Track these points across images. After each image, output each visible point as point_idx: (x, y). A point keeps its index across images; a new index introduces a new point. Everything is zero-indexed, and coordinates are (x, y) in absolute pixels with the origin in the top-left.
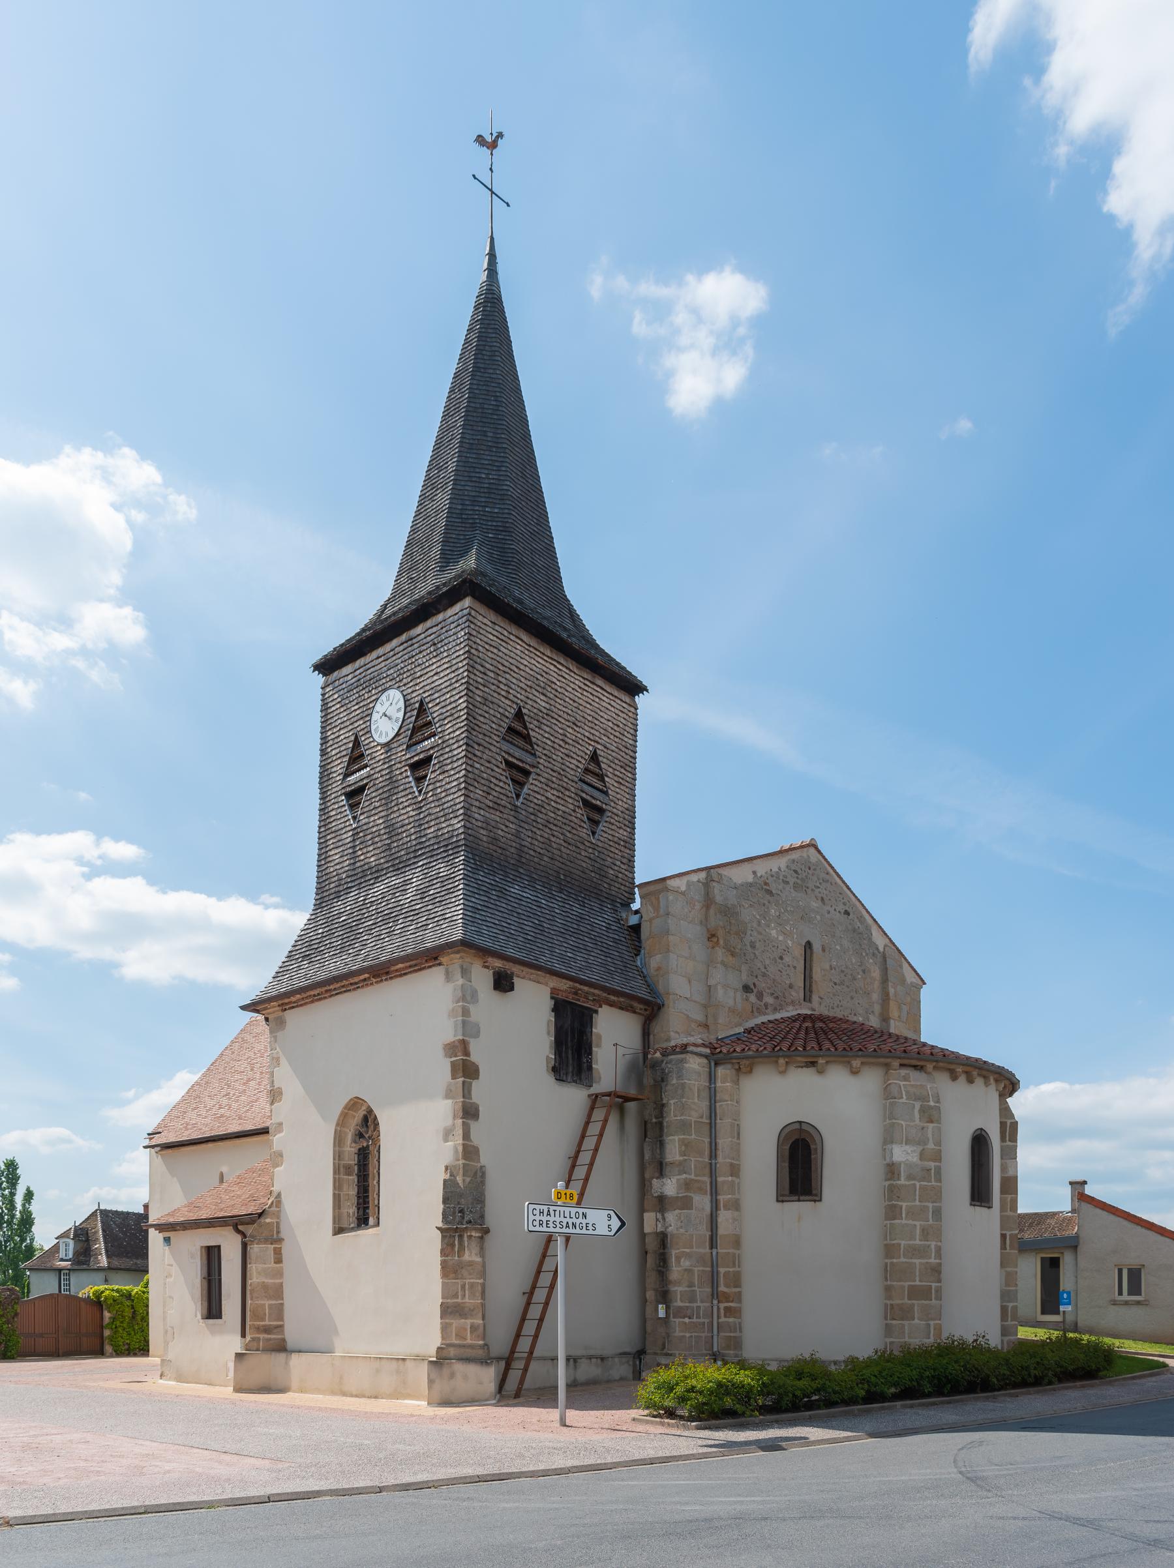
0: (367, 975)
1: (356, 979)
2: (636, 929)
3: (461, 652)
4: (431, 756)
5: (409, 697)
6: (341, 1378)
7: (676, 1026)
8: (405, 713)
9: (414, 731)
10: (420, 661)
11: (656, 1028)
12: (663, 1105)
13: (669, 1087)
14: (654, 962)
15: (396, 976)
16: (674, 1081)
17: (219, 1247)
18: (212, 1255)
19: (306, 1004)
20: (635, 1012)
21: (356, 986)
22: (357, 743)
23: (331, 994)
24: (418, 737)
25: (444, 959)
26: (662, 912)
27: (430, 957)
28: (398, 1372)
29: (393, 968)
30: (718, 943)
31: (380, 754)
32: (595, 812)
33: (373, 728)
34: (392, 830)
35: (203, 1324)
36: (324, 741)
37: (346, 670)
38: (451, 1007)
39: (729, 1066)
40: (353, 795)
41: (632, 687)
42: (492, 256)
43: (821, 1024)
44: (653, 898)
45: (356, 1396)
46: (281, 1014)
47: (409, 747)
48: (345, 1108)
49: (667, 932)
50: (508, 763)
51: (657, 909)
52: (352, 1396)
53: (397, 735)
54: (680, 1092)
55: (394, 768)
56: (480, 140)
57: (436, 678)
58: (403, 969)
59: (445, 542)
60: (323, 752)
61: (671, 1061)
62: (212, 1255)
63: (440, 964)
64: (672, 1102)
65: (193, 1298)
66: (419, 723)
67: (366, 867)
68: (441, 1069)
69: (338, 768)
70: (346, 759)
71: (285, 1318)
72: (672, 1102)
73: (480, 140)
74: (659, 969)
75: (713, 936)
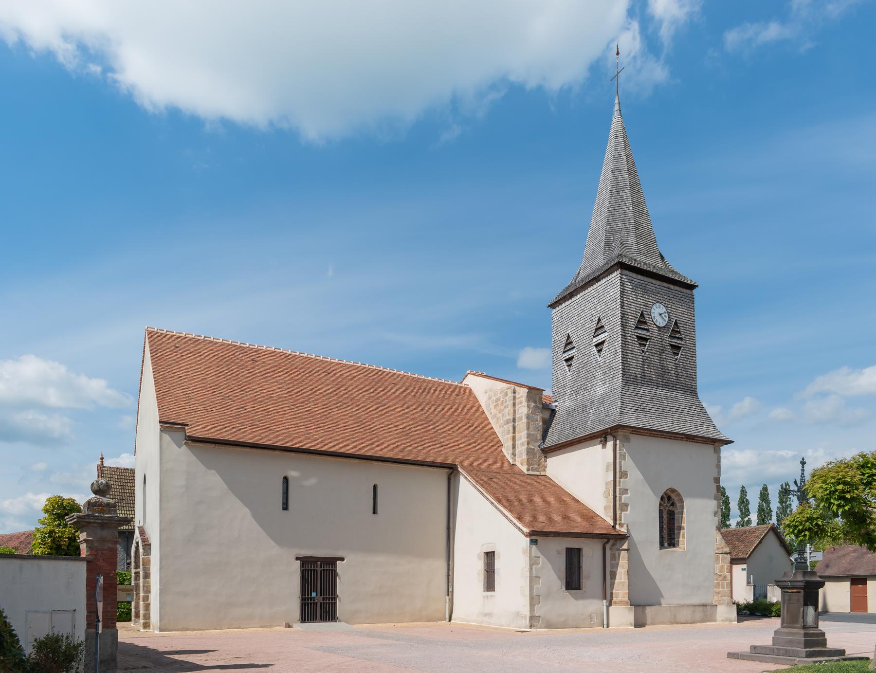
9: (597, 330)
35: (567, 593)
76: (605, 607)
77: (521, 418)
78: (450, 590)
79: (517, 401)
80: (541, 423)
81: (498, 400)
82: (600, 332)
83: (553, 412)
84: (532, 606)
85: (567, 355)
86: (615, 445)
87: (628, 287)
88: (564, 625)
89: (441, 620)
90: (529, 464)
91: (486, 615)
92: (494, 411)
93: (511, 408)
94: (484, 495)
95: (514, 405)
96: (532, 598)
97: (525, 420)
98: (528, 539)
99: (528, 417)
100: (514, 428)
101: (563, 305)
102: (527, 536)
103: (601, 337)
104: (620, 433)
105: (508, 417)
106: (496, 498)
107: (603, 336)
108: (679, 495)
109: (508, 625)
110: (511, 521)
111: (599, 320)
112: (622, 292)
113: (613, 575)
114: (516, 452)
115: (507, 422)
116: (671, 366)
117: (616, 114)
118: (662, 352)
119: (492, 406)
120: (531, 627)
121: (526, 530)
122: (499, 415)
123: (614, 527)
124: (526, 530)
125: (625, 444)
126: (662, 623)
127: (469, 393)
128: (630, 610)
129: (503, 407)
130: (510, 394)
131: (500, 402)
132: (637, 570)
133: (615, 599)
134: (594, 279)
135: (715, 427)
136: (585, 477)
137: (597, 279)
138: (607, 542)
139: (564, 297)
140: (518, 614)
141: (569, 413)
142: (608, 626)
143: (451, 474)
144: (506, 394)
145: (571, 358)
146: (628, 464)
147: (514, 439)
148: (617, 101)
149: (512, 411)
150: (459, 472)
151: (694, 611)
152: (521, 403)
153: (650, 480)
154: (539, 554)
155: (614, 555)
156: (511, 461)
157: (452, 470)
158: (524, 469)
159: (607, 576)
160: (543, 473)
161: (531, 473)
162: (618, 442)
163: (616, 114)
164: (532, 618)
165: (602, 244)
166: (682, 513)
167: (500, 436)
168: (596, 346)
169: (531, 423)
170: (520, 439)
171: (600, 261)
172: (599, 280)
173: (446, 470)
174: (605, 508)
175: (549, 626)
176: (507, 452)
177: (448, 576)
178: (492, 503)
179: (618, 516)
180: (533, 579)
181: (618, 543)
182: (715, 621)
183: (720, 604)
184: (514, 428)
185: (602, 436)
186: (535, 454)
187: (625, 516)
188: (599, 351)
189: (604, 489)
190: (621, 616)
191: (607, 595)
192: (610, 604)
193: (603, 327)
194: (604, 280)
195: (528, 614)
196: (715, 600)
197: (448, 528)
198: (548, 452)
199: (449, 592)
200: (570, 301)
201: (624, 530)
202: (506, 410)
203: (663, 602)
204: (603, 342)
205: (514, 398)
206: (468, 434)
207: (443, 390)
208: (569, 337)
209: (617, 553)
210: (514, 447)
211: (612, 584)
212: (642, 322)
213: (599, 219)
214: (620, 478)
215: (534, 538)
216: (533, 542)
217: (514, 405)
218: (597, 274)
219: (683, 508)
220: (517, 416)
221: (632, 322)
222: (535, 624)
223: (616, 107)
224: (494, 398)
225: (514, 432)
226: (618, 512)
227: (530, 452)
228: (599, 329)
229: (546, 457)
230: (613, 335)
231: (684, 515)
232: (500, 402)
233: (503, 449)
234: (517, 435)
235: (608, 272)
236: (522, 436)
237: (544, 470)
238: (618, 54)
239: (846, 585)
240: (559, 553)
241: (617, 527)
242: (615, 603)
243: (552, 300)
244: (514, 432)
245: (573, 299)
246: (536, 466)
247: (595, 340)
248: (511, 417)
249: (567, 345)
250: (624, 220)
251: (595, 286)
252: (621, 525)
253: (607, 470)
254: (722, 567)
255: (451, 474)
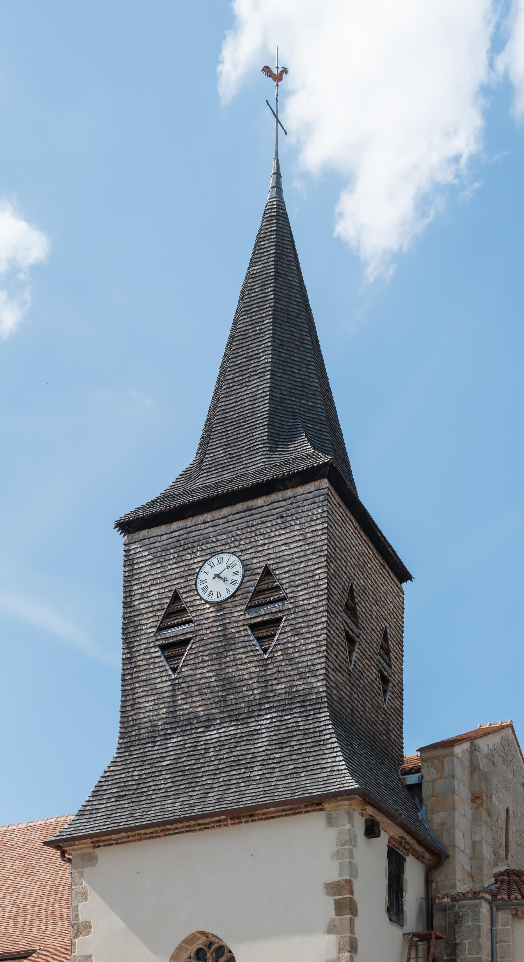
1: (207, 820)
2: (415, 789)
3: (319, 527)
4: (281, 618)
5: (248, 562)
7: (460, 876)
8: (244, 577)
9: (257, 593)
10: (263, 531)
11: (439, 876)
12: (456, 945)
13: (463, 929)
14: (437, 818)
15: (261, 819)
16: (470, 923)
20: (423, 862)
22: (176, 598)
23: (166, 833)
24: (260, 599)
25: (326, 806)
26: (446, 774)
27: (315, 803)
29: (258, 812)
30: (482, 804)
31: (210, 612)
32: (385, 680)
33: (200, 587)
34: (227, 684)
36: (128, 593)
37: (162, 529)
38: (335, 849)
39: (508, 911)
40: (172, 650)
41: (403, 575)
42: (278, 175)
43: (515, 878)
44: (436, 762)
46: (90, 850)
47: (248, 608)
48: (183, 942)
49: (453, 792)
50: (347, 633)
51: (441, 771)
53: (233, 595)
54: (475, 933)
55: (229, 626)
56: (267, 70)
57: (283, 548)
58: (273, 812)
59: (271, 425)
60: (127, 605)
61: (464, 906)
63: (321, 810)
64: (466, 942)
66: (263, 587)
67: (192, 716)
68: (327, 906)
69: (149, 623)
70: (162, 613)
72: (466, 942)
73: (267, 70)
74: (443, 824)
75: (477, 798)
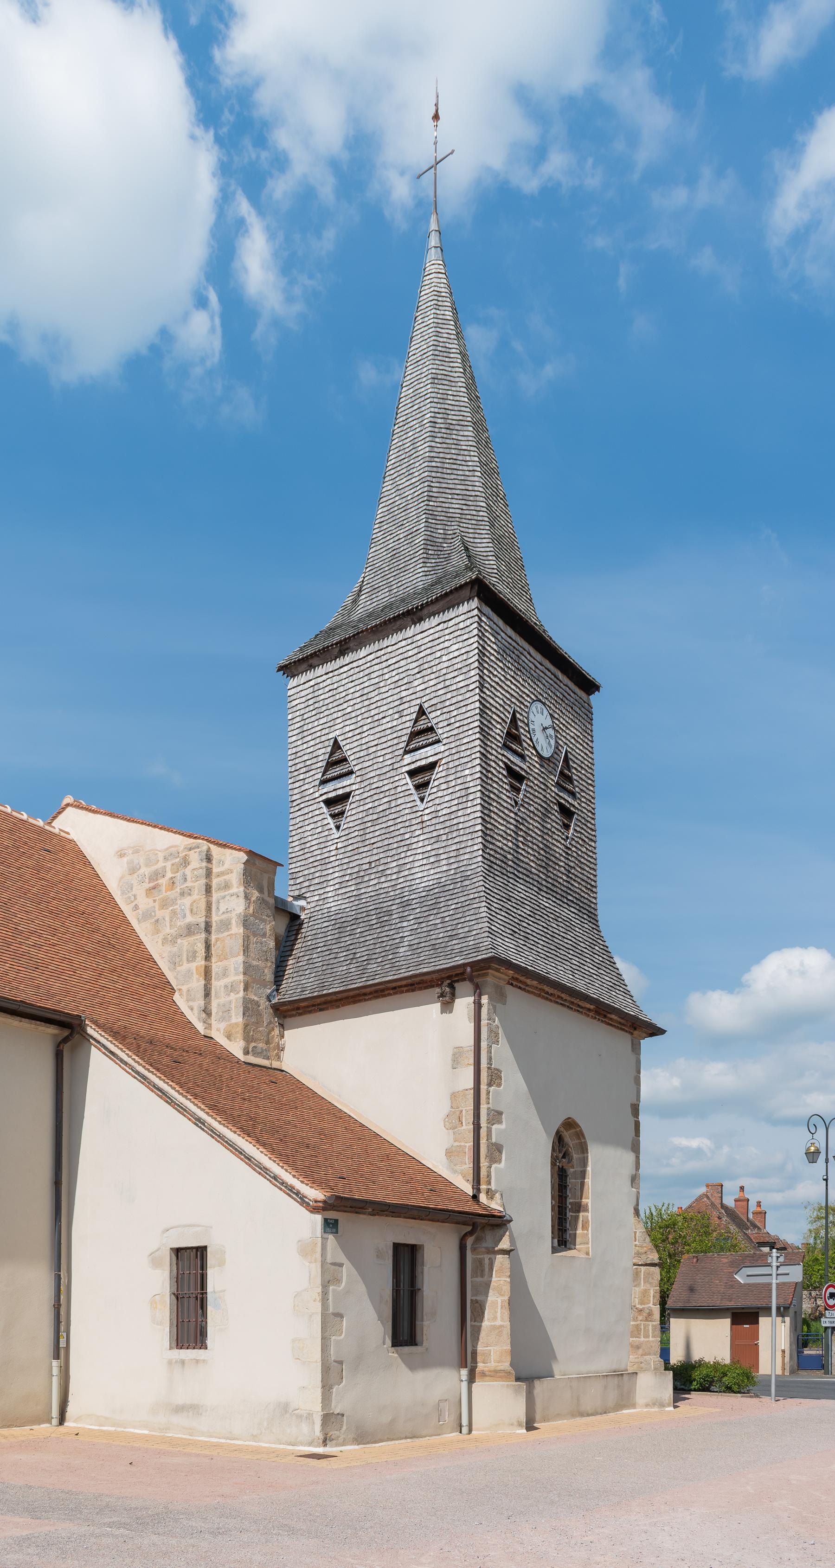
0: (592, 1007)
6: (578, 1400)
9: (414, 735)
17: (421, 1247)
18: (406, 1259)
19: (532, 993)
21: (579, 1009)
28: (619, 1386)
35: (393, 1355)
45: (592, 1415)
52: (588, 1415)
62: (406, 1259)
63: (632, 1034)
65: (380, 1318)
71: (783, 1402)
76: (464, 1385)
77: (225, 925)
78: (63, 1344)
79: (215, 882)
80: (272, 944)
81: (157, 875)
82: (421, 740)
83: (294, 921)
84: (327, 1388)
85: (333, 789)
86: (478, 1006)
87: (492, 648)
88: (389, 1433)
89: (38, 1421)
90: (248, 1039)
91: (179, 1409)
92: (144, 903)
93: (198, 896)
94: (170, 1101)
95: (208, 889)
96: (326, 1369)
97: (237, 930)
98: (318, 1218)
99: (246, 923)
100: (208, 947)
101: (320, 671)
102: (314, 1210)
103: (425, 756)
104: (491, 978)
105: (190, 919)
106: (214, 1108)
107: (430, 750)
108: (580, 1135)
109: (254, 1437)
110: (263, 1171)
111: (421, 712)
112: (482, 654)
113: (479, 1314)
114: (216, 1004)
115: (190, 930)
116: (559, 849)
117: (433, 255)
118: (545, 815)
119: (140, 890)
120: (325, 1443)
121: (314, 1194)
122: (159, 914)
123: (475, 1197)
124: (314, 1194)
125: (499, 1006)
126: (558, 1416)
127: (68, 851)
128: (517, 1391)
129: (171, 894)
130: (196, 862)
131: (163, 882)
132: (521, 1303)
133: (481, 1366)
134: (408, 613)
135: (627, 993)
136: (401, 1077)
137: (415, 615)
138: (470, 1233)
139: (325, 650)
140: (284, 1409)
141: (341, 925)
142: (470, 1431)
143: (65, 1040)
144: (186, 862)
145: (344, 798)
146: (502, 1054)
147: (207, 973)
148: (433, 226)
149: (203, 905)
150: (86, 1037)
151: (605, 1388)
152: (227, 886)
153: (539, 1095)
154: (342, 1258)
155: (480, 1262)
156: (200, 1027)
157: (68, 1034)
158: (236, 1048)
159: (468, 1313)
160: (275, 1064)
161: (251, 1059)
162: (485, 1000)
163: (433, 255)
164: (329, 1419)
165: (419, 540)
166: (583, 1174)
167: (164, 966)
168: (412, 773)
169: (253, 940)
170: (225, 974)
171: (415, 579)
172: (420, 620)
173: (52, 1030)
174: (449, 1153)
175: (363, 1437)
176: (188, 1005)
177: (57, 1307)
178: (199, 1122)
179: (483, 1172)
180: (330, 1319)
181: (489, 1236)
182: (633, 1406)
183: (643, 1370)
184: (208, 947)
185: (444, 984)
186: (259, 1014)
187: (498, 1174)
188: (421, 787)
189: (445, 1107)
190: (496, 1403)
191: (467, 1359)
192: (471, 1379)
193: (431, 729)
194: (435, 621)
195: (317, 1408)
196: (629, 1361)
197: (57, 1183)
198: (290, 1012)
199: (60, 1350)
200: (340, 662)
201: (495, 1205)
202: (187, 901)
203: (557, 1369)
204: (432, 766)
205: (209, 873)
206: (90, 947)
207: (11, 831)
208: (336, 746)
209: (486, 1257)
210: (207, 995)
211: (477, 1331)
212: (513, 737)
213: (403, 482)
214: (490, 1085)
215: (332, 1215)
216: (330, 1226)
217: (208, 889)
218: (417, 603)
219: (584, 1162)
220: (215, 918)
221: (498, 731)
222: (334, 1433)
223: (434, 241)
224: (145, 871)
225: (208, 957)
226: (484, 1163)
227: (249, 1008)
228: (422, 733)
229: (282, 1026)
230: (460, 755)
231: (588, 1180)
232: (163, 882)
233: (176, 997)
234: (216, 966)
235: (447, 600)
236: (231, 968)
237: (278, 1058)
238: (436, 117)
239: (725, 1324)
240: (379, 1255)
241: (483, 1198)
242: (483, 1374)
243: (290, 652)
244: (208, 957)
245: (348, 659)
246: (261, 1045)
247: (408, 758)
248: (201, 920)
249: (330, 765)
250: (464, 498)
251: (410, 632)
252: (490, 1194)
253: (456, 1061)
254: (645, 1293)
255: (65, 1040)
